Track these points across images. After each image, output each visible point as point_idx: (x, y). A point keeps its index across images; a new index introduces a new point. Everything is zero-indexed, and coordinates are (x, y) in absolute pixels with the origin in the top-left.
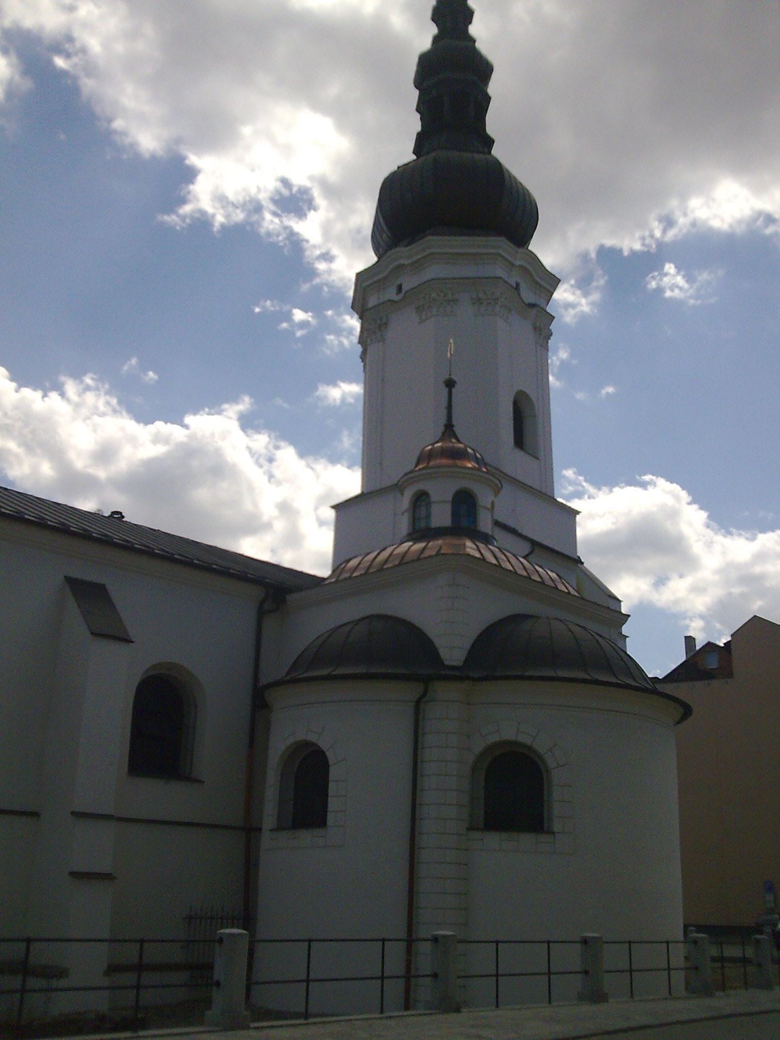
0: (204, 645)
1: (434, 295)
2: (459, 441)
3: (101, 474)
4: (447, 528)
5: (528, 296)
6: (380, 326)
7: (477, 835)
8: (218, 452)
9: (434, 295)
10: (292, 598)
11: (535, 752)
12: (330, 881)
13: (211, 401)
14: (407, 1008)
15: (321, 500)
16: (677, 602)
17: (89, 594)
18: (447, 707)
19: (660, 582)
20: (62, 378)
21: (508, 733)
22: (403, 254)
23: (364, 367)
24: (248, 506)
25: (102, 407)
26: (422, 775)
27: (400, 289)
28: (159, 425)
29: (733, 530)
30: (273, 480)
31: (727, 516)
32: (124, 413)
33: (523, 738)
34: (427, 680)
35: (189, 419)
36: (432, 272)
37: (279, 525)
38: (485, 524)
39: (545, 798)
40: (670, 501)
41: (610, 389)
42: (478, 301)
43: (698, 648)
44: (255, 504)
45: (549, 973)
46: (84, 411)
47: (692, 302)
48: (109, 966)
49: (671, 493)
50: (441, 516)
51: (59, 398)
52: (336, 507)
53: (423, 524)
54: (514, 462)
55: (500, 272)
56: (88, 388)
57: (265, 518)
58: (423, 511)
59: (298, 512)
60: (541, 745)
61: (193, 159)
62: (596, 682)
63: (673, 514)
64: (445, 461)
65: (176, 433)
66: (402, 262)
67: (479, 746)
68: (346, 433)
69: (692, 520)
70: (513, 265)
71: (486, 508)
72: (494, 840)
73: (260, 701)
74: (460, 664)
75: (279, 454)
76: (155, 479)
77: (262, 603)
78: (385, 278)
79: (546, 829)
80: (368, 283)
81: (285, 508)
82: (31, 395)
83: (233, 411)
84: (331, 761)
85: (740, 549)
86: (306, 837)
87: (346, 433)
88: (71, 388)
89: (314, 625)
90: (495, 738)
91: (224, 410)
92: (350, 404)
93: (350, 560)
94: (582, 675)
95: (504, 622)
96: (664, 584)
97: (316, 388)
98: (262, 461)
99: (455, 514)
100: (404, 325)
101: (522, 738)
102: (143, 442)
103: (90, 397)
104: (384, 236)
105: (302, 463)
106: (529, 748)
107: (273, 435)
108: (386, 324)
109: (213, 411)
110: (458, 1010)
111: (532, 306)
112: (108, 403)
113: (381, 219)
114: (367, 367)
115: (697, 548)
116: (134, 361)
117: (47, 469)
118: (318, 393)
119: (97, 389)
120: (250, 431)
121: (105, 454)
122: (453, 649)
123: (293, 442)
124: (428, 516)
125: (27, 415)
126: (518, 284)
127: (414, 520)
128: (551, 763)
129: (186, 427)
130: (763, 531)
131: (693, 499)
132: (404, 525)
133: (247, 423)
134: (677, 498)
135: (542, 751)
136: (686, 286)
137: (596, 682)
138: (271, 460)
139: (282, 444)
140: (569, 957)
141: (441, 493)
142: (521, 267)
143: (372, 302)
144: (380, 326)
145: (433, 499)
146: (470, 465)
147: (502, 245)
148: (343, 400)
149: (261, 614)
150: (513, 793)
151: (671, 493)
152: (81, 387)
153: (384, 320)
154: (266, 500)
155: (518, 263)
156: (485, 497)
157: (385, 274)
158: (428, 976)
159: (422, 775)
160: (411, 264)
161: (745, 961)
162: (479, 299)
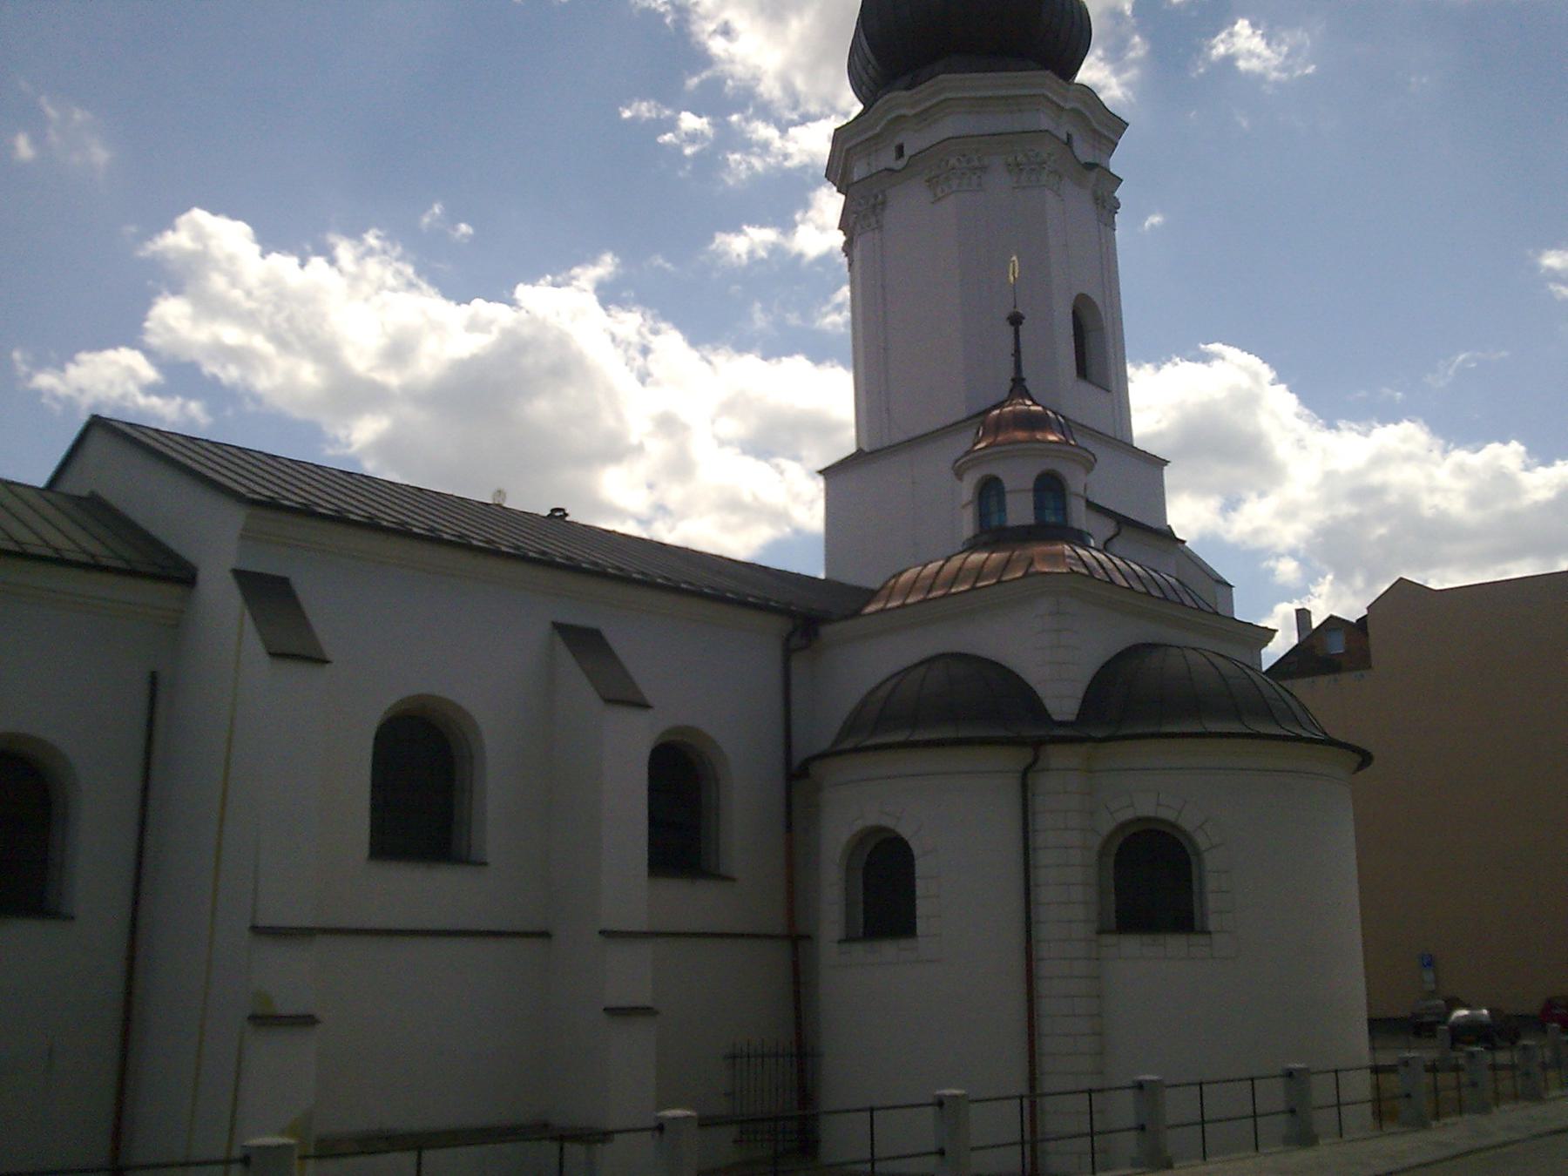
0: (710, 690)
1: (953, 161)
2: (1035, 403)
3: (393, 379)
5: (1084, 151)
6: (874, 206)
7: (1112, 939)
8: (563, 341)
9: (953, 161)
10: (827, 631)
13: (554, 263)
15: (729, 408)
16: (1257, 532)
17: (584, 642)
19: (1231, 505)
20: (332, 238)
22: (901, 101)
23: (850, 265)
24: (609, 422)
25: (391, 281)
26: (1037, 885)
27: (900, 151)
28: (478, 304)
30: (649, 380)
31: (1331, 397)
32: (424, 286)
33: (1168, 815)
34: (1038, 744)
35: (523, 292)
36: (948, 127)
37: (658, 449)
38: (1080, 518)
39: (1195, 888)
40: (1245, 382)
41: (1155, 219)
43: (1315, 625)
44: (619, 417)
45: (1255, 1115)
46: (366, 288)
47: (1274, 75)
49: (1245, 369)
50: (1019, 511)
51: (326, 265)
52: (826, 472)
53: (995, 522)
54: (1078, 401)
55: (1045, 121)
56: (370, 252)
57: (634, 439)
59: (685, 428)
60: (1188, 822)
63: (1248, 401)
64: (1020, 435)
65: (497, 314)
66: (903, 111)
67: (1106, 825)
68: (758, 306)
69: (1278, 412)
70: (1062, 109)
71: (1077, 495)
72: (1132, 944)
74: (1072, 718)
75: (655, 342)
76: (480, 391)
77: (788, 640)
78: (878, 135)
79: (1197, 924)
80: (853, 142)
81: (667, 424)
82: (283, 265)
83: (588, 276)
84: (916, 851)
85: (1350, 449)
86: (889, 949)
87: (758, 306)
88: (345, 251)
89: (865, 665)
90: (1128, 815)
91: (574, 278)
92: (762, 260)
93: (900, 574)
94: (1235, 727)
95: (1121, 656)
96: (1234, 509)
97: (712, 239)
98: (633, 352)
99: (1039, 507)
100: (909, 203)
102: (456, 332)
103: (373, 267)
104: (871, 71)
105: (694, 355)
106: (1173, 826)
107: (649, 314)
108: (883, 203)
109: (559, 279)
110: (1169, 1166)
111: (1090, 166)
112: (399, 273)
113: (863, 38)
114: (857, 264)
115: (1281, 448)
116: (437, 209)
117: (309, 374)
118: (714, 246)
119: (385, 252)
120: (614, 309)
121: (398, 351)
122: (1062, 698)
123: (680, 326)
125: (281, 295)
126: (1069, 136)
127: (983, 516)
129: (512, 303)
130: (1384, 422)
131: (1279, 374)
132: (967, 526)
133: (609, 295)
134: (1255, 377)
136: (1267, 53)
138: (645, 351)
139: (663, 326)
140: (1273, 1095)
141: (1018, 478)
142: (1072, 110)
143: (859, 172)
145: (1008, 486)
146: (1052, 438)
147: (1045, 81)
148: (751, 253)
149: (788, 653)
150: (1153, 883)
151: (1245, 369)
152: (362, 249)
154: (634, 411)
155: (1068, 106)
156: (1076, 481)
158: (1129, 1129)
159: (1037, 885)
160: (915, 115)
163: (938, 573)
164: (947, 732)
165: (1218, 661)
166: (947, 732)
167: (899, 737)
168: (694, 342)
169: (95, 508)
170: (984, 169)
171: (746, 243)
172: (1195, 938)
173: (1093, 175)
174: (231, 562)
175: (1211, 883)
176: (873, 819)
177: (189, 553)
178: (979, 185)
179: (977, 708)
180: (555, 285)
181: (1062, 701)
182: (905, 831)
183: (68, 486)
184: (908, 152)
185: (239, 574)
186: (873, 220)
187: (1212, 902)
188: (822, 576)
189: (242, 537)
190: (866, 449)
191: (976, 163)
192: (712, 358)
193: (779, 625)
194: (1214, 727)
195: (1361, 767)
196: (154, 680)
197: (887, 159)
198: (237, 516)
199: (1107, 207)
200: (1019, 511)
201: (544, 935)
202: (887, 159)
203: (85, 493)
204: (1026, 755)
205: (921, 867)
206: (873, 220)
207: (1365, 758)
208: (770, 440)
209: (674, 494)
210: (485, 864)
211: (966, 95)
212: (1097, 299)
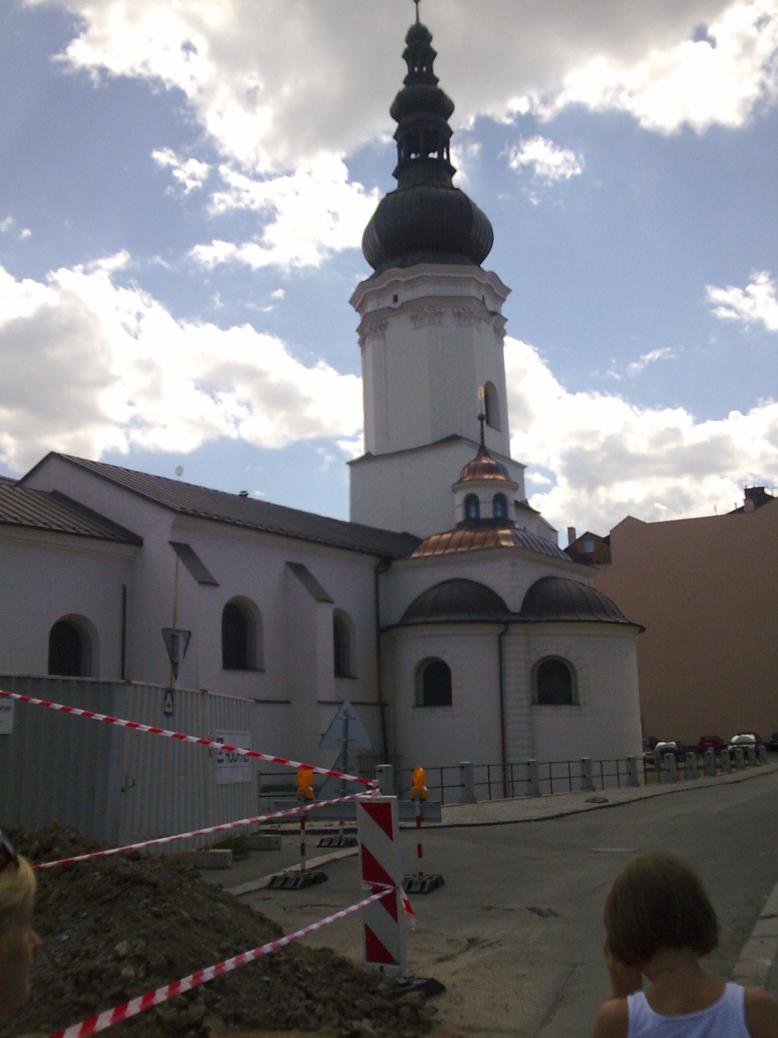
5: (490, 305)
6: (380, 327)
7: (538, 707)
9: (425, 309)
10: (396, 564)
12: (457, 734)
13: (76, 254)
14: (505, 796)
17: (299, 570)
21: (552, 651)
22: (395, 273)
27: (396, 299)
29: (606, 393)
34: (507, 623)
35: (62, 275)
36: (422, 291)
42: (458, 315)
43: (578, 537)
53: (473, 515)
55: (473, 291)
58: (473, 508)
60: (571, 658)
61: (563, 543)
62: (602, 622)
67: (535, 658)
72: (547, 709)
78: (382, 290)
86: (439, 711)
89: (416, 580)
90: (544, 654)
100: (400, 329)
106: (564, 659)
108: (386, 325)
116: (9, 220)
122: (514, 602)
124: (478, 511)
126: (483, 297)
128: (577, 667)
132: (459, 516)
137: (602, 622)
141: (486, 496)
142: (488, 285)
143: (370, 307)
149: (377, 573)
150: (555, 683)
153: (384, 322)
157: (384, 286)
161: (685, 769)
162: (459, 313)
164: (465, 617)
165: (580, 586)
166: (465, 617)
167: (444, 618)
168: (177, 314)
169: (58, 497)
170: (441, 314)
171: (213, 253)
172: (574, 707)
173: (494, 319)
174: (167, 536)
175: (580, 683)
177: (138, 532)
179: (473, 605)
180: (86, 272)
181: (514, 603)
182: (446, 659)
183: (31, 485)
184: (401, 300)
185: (171, 543)
187: (581, 691)
188: (342, 512)
189: (172, 527)
190: (374, 453)
192: (186, 325)
193: (372, 561)
194: (583, 617)
195: (640, 632)
196: (124, 588)
197: (388, 302)
198: (168, 518)
199: (500, 333)
200: (486, 511)
201: (287, 702)
203: (50, 491)
204: (501, 628)
205: (454, 675)
206: (380, 333)
207: (642, 629)
209: (145, 409)
210: (264, 671)
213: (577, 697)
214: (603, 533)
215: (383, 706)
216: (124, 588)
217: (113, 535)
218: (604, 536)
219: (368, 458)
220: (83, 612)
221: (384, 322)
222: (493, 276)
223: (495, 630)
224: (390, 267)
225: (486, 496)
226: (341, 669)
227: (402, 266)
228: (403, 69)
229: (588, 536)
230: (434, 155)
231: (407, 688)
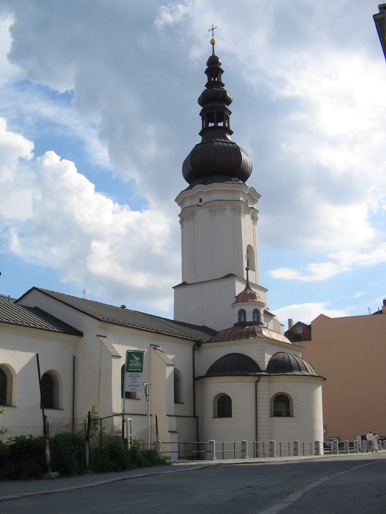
1: (217, 207)
4: (251, 322)
6: (192, 214)
9: (217, 207)
10: (203, 345)
11: (289, 395)
18: (263, 385)
22: (199, 187)
26: (268, 410)
27: (201, 200)
43: (294, 324)
48: (46, 417)
58: (242, 317)
60: (290, 393)
67: (273, 394)
72: (277, 419)
73: (196, 379)
78: (193, 195)
79: (291, 415)
86: (225, 419)
89: (215, 352)
101: (285, 392)
108: (195, 214)
124: (245, 318)
135: (290, 395)
144: (192, 214)
149: (194, 350)
150: (282, 406)
159: (268, 410)
163: (231, 333)
169: (37, 311)
170: (225, 209)
175: (294, 406)
176: (221, 391)
178: (224, 213)
183: (23, 302)
186: (192, 218)
191: (223, 208)
193: (192, 344)
196: (74, 357)
197: (197, 202)
200: (249, 318)
202: (197, 202)
203: (33, 307)
205: (233, 402)
207: (325, 379)
208: (145, 260)
211: (221, 189)
212: (252, 245)
213: (292, 413)
214: (308, 322)
215: (195, 416)
216: (74, 357)
217: (63, 330)
218: (308, 324)
219: (184, 284)
220: (55, 369)
221: (194, 213)
222: (253, 190)
223: (253, 379)
224: (197, 184)
225: (249, 309)
226: (177, 400)
227: (205, 183)
228: (205, 79)
229: (299, 324)
230: (221, 124)
231: (210, 407)
